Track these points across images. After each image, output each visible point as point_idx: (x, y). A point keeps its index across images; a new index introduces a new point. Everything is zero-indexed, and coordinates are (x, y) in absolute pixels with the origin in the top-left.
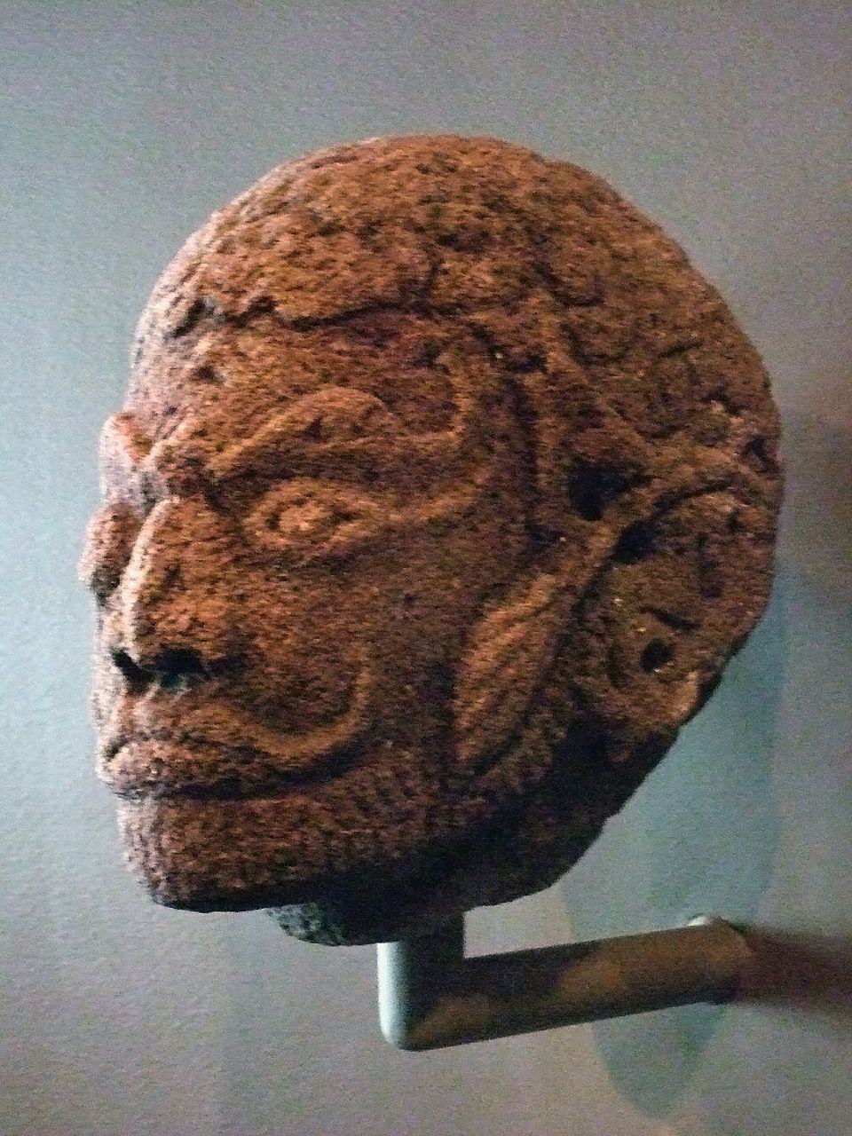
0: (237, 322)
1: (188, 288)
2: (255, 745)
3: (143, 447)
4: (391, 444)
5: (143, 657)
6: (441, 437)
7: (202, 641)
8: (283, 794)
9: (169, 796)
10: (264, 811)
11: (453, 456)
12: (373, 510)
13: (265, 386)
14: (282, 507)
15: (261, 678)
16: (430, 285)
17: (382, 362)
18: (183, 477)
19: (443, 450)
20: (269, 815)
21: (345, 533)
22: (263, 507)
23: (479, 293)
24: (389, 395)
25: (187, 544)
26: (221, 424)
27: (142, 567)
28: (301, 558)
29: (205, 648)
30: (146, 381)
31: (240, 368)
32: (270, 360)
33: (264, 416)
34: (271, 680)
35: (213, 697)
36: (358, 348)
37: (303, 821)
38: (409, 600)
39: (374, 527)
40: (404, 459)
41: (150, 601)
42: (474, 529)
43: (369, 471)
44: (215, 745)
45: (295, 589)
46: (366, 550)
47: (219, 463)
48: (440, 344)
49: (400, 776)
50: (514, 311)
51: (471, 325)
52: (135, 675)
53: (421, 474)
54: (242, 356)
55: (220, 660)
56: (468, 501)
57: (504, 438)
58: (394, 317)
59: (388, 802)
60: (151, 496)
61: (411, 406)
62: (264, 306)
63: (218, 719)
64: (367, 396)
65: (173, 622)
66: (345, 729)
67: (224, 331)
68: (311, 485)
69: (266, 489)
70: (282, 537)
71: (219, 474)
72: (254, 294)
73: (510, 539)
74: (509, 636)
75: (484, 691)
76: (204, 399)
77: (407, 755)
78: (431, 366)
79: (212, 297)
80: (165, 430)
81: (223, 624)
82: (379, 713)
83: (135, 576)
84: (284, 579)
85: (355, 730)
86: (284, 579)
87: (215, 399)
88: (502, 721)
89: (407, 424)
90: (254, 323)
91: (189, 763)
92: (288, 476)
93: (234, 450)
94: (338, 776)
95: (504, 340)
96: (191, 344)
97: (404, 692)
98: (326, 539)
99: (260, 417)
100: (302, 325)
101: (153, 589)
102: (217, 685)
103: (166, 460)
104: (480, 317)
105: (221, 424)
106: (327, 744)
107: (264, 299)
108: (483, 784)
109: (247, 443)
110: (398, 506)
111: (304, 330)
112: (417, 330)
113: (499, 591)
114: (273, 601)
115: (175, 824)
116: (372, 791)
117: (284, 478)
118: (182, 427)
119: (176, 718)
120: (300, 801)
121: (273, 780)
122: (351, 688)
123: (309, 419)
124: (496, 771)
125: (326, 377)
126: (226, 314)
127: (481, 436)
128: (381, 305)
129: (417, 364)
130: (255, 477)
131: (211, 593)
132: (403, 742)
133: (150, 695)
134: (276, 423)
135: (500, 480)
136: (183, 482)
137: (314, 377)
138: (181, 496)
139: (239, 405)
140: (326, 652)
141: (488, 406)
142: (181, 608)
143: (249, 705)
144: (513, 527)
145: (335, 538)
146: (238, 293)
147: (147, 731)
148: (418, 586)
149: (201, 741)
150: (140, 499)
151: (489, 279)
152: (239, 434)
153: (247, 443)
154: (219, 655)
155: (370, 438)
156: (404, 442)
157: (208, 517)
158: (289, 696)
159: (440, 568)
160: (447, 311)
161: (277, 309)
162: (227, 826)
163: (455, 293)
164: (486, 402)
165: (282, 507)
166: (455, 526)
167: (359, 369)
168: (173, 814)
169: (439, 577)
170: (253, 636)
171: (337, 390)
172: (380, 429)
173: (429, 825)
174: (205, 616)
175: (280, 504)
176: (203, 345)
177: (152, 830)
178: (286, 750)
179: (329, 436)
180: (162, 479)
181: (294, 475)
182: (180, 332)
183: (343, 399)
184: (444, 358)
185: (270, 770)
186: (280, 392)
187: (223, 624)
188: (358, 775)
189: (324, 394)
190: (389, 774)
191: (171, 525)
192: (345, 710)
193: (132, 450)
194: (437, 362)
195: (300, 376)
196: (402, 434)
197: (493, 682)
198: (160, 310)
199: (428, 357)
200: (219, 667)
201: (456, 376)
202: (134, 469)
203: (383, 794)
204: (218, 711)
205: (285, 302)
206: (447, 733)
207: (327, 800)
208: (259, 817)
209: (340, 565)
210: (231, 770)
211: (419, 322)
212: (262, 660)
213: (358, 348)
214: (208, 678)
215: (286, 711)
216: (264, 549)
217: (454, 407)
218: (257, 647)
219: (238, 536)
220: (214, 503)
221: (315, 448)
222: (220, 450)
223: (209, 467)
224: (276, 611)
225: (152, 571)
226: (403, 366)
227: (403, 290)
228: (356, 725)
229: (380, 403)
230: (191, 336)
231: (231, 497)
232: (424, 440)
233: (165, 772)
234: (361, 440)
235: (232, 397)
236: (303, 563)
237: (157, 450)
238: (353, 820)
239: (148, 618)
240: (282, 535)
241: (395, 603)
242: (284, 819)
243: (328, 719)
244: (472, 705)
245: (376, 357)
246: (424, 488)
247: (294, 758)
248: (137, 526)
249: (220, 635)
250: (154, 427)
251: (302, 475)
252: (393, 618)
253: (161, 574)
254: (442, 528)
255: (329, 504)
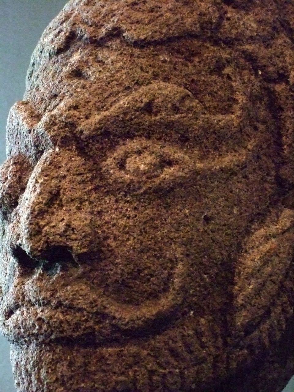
0: (97, 43)
1: (66, 26)
2: (106, 311)
3: (36, 119)
4: (197, 119)
5: (33, 250)
6: (228, 117)
7: (73, 240)
8: (123, 344)
9: (48, 344)
10: (110, 355)
11: (234, 130)
12: (185, 161)
13: (116, 80)
14: (127, 155)
15: (112, 266)
16: (219, 25)
17: (190, 68)
18: (63, 134)
19: (228, 125)
20: (113, 358)
21: (168, 173)
22: (115, 155)
23: (248, 33)
24: (195, 89)
25: (64, 177)
26: (88, 102)
27: (35, 191)
28: (140, 188)
29: (75, 245)
30: (38, 82)
31: (101, 69)
32: (120, 64)
33: (114, 99)
34: (117, 269)
35: (79, 278)
36: (175, 60)
37: (136, 363)
38: (207, 220)
39: (187, 170)
40: (205, 130)
41: (39, 214)
42: (246, 177)
43: (182, 136)
44: (80, 310)
45: (136, 209)
46: (181, 185)
47: (84, 127)
48: (224, 61)
49: (198, 334)
50: (268, 46)
51: (244, 52)
52: (25, 262)
53: (213, 140)
54: (101, 63)
55: (84, 253)
56: (243, 159)
57: (264, 122)
58: (197, 43)
59: (191, 352)
60: (40, 149)
61: (208, 97)
62: (116, 33)
63: (81, 293)
64: (181, 89)
65: (54, 227)
66: (166, 302)
67: (90, 48)
68: (145, 142)
69: (117, 143)
70: (127, 174)
71: (86, 133)
72: (109, 26)
73: (267, 186)
74: (268, 246)
75: (253, 281)
76: (77, 87)
77: (203, 321)
78: (220, 75)
79: (81, 28)
80: (50, 107)
81: (88, 230)
82: (187, 292)
83: (29, 198)
84: (128, 202)
85: (173, 303)
86: (128, 202)
87: (84, 87)
88: (263, 301)
89: (206, 108)
90: (109, 43)
91: (61, 322)
92: (130, 136)
93: (96, 118)
94: (159, 333)
95: (264, 61)
96: (68, 58)
97: (202, 279)
98: (156, 176)
99: (112, 99)
100: (139, 44)
101: (41, 205)
102: (81, 270)
103: (49, 126)
104: (249, 47)
105: (88, 102)
106: (154, 312)
107: (114, 29)
108: (247, 341)
109: (106, 113)
110: (202, 158)
111: (142, 47)
112: (211, 53)
113: (260, 217)
114: (119, 216)
115: (50, 363)
116: (180, 344)
117: (128, 137)
118: (62, 104)
119: (54, 292)
120: (134, 349)
121: (117, 335)
122: (170, 275)
123: (146, 100)
124: (256, 333)
125: (156, 76)
126: (91, 38)
127: (251, 120)
128: (191, 35)
129: (211, 72)
130: (110, 135)
131: (79, 208)
132: (200, 312)
133: (36, 276)
134: (124, 102)
135: (261, 147)
136: (62, 138)
137: (149, 75)
138: (60, 147)
139: (99, 91)
140: (155, 250)
141: (254, 103)
142: (60, 218)
143: (103, 283)
144: (269, 178)
145: (162, 176)
146: (97, 26)
147: (33, 300)
148: (213, 210)
149: (70, 307)
150: (33, 151)
151: (254, 25)
152: (99, 109)
153: (106, 113)
154: (85, 250)
155: (183, 115)
156: (205, 118)
157: (78, 160)
158: (129, 278)
159: (226, 200)
160: (229, 43)
161: (124, 35)
162: (86, 364)
163: (234, 32)
164: (253, 99)
165: (127, 155)
166: (236, 174)
167: (177, 73)
168: (49, 356)
169: (225, 206)
170: (106, 238)
171: (162, 84)
172: (190, 109)
173: (215, 367)
174: (75, 223)
175: (126, 153)
176: (76, 57)
177: (34, 366)
178: (126, 315)
179: (158, 111)
180: (48, 136)
181: (135, 136)
182: (59, 51)
183: (168, 90)
184: (228, 70)
185: (116, 328)
186: (127, 84)
187: (88, 230)
188: (171, 333)
189: (155, 86)
190: (191, 333)
191: (54, 165)
192: (165, 290)
193: (29, 120)
194: (223, 72)
195: (138, 74)
196: (204, 114)
197: (258, 275)
198: (48, 40)
199: (218, 69)
200: (83, 258)
201: (235, 81)
202: (30, 132)
203: (187, 346)
204: (84, 288)
205: (129, 30)
206: (228, 307)
207: (152, 350)
208: (107, 359)
209: (163, 194)
210: (90, 327)
211: (212, 48)
212: (112, 255)
213: (175, 60)
214: (76, 266)
215: (126, 289)
216: (115, 181)
217: (235, 101)
218: (109, 245)
219: (98, 174)
220: (82, 151)
221: (148, 119)
222: (87, 118)
223: (79, 128)
224: (122, 222)
225: (41, 193)
226: (203, 73)
227: (202, 28)
228: (173, 299)
229: (190, 93)
230: (68, 53)
231: (94, 148)
232: (216, 118)
233: (45, 327)
234: (178, 116)
235: (95, 86)
236: (142, 191)
237: (45, 118)
238: (168, 363)
239: (37, 224)
240: (127, 172)
241: (198, 220)
242: (123, 360)
243: (154, 296)
244: (245, 289)
245: (187, 66)
246: (216, 149)
247: (132, 320)
248: (30, 168)
249: (85, 237)
250: (43, 106)
251: (140, 136)
252: (198, 230)
253: (46, 196)
254: (229, 173)
255: (158, 154)
